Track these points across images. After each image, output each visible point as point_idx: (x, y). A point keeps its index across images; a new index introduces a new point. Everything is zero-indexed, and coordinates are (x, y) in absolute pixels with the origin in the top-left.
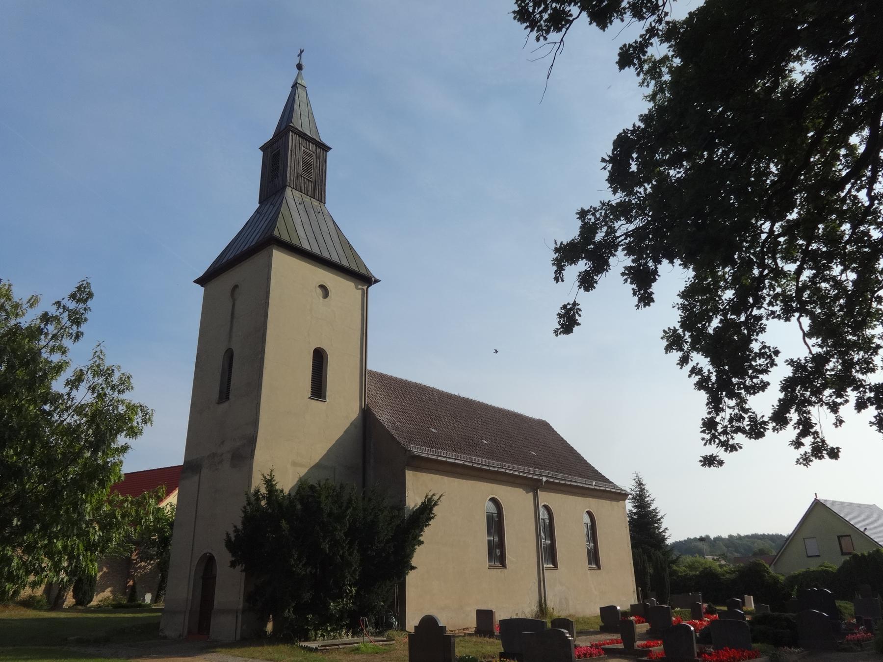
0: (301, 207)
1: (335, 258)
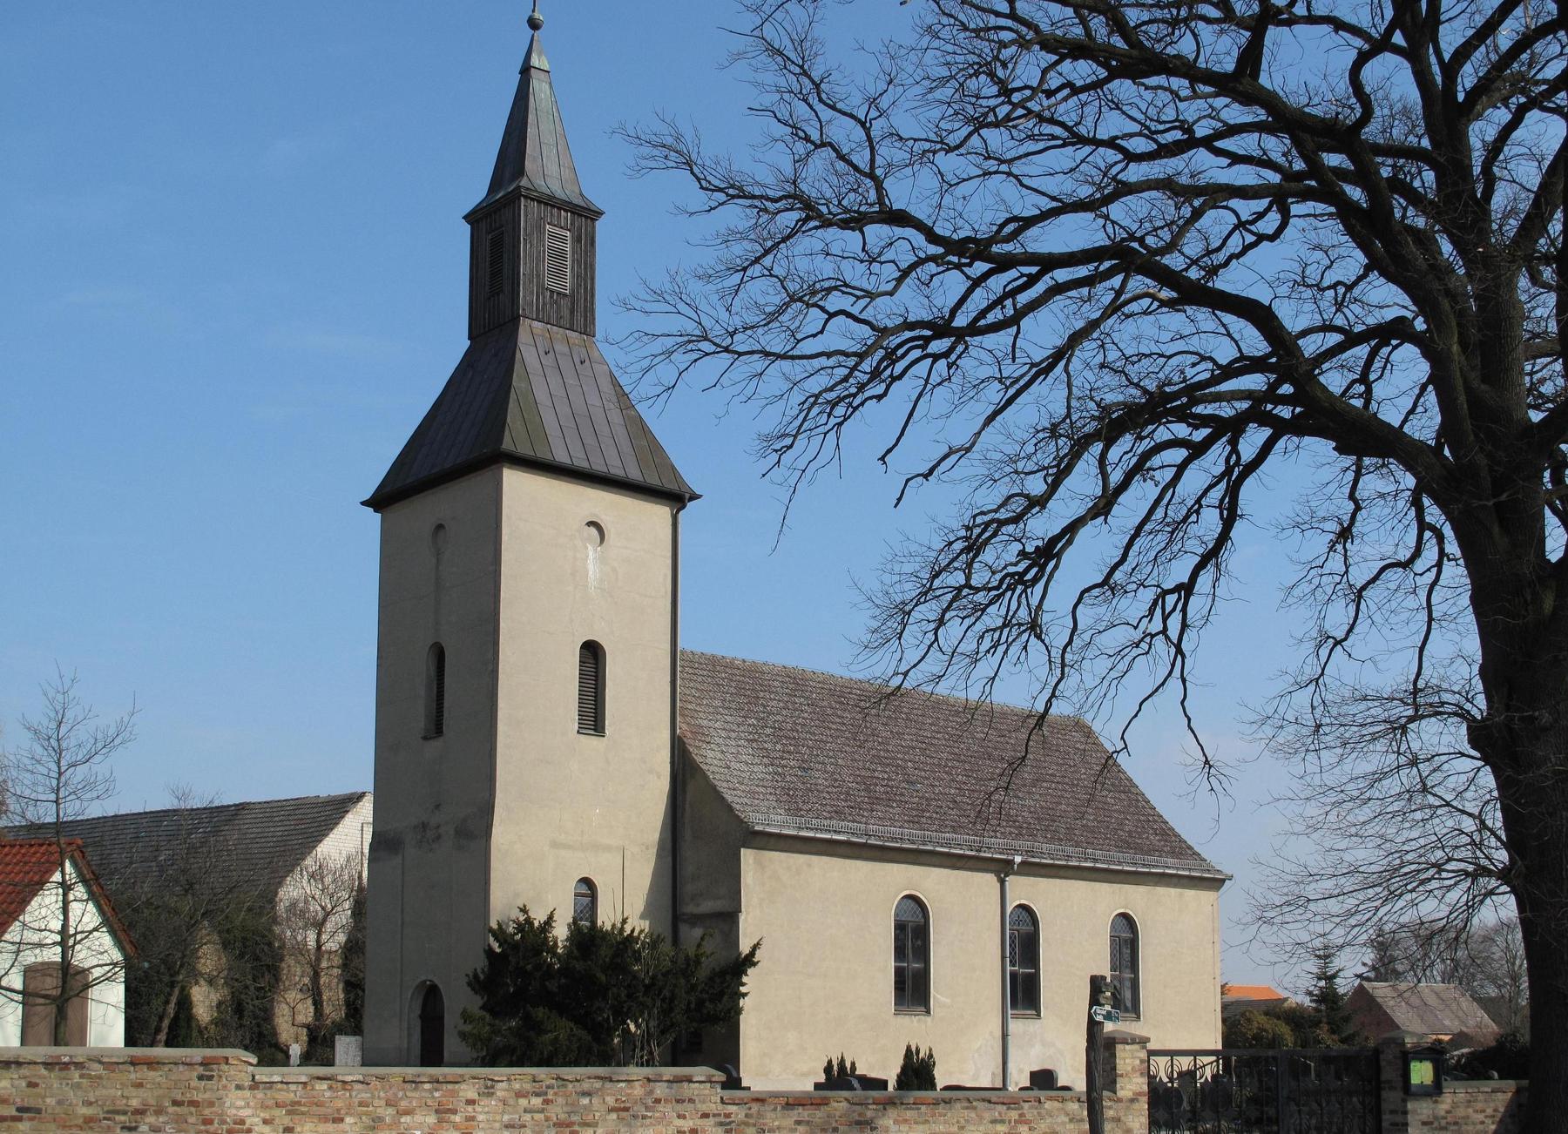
0: (548, 361)
1: (616, 471)
